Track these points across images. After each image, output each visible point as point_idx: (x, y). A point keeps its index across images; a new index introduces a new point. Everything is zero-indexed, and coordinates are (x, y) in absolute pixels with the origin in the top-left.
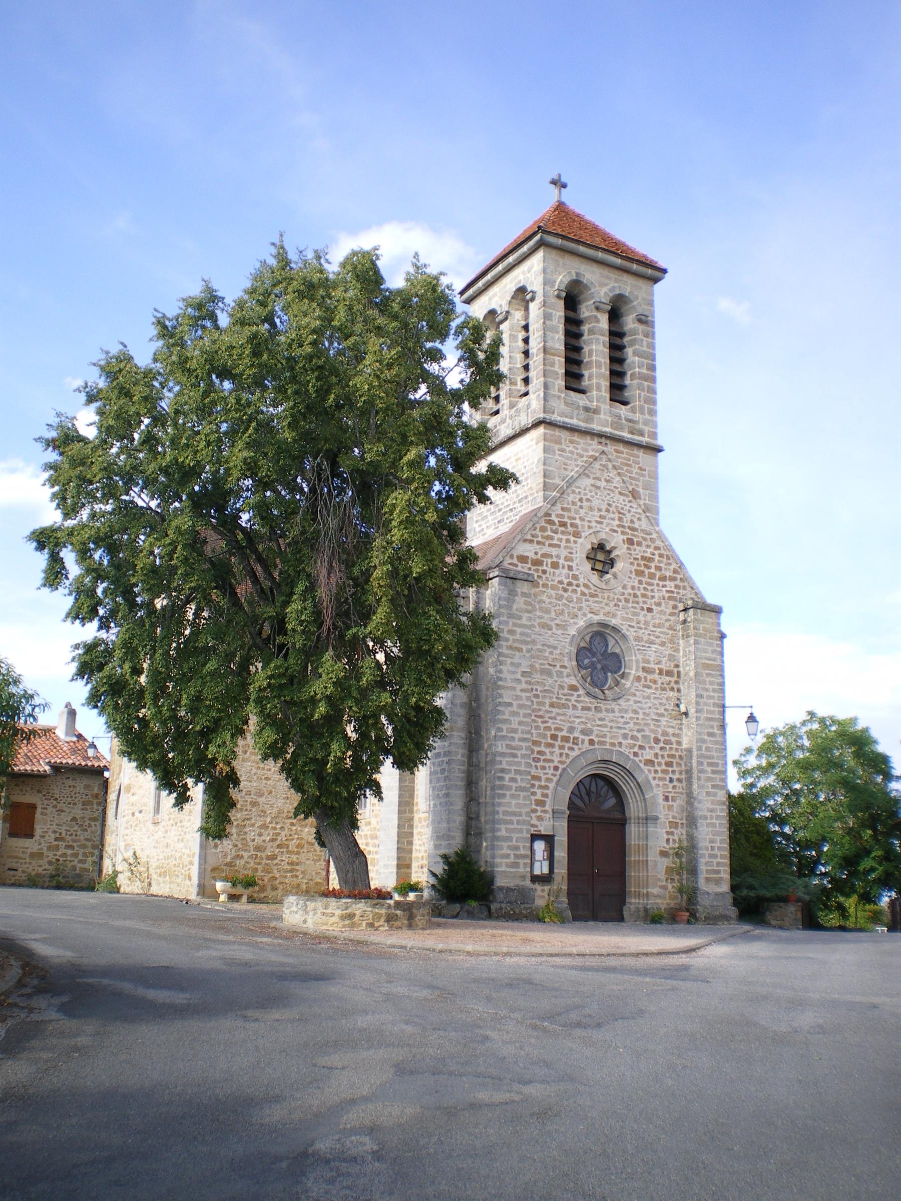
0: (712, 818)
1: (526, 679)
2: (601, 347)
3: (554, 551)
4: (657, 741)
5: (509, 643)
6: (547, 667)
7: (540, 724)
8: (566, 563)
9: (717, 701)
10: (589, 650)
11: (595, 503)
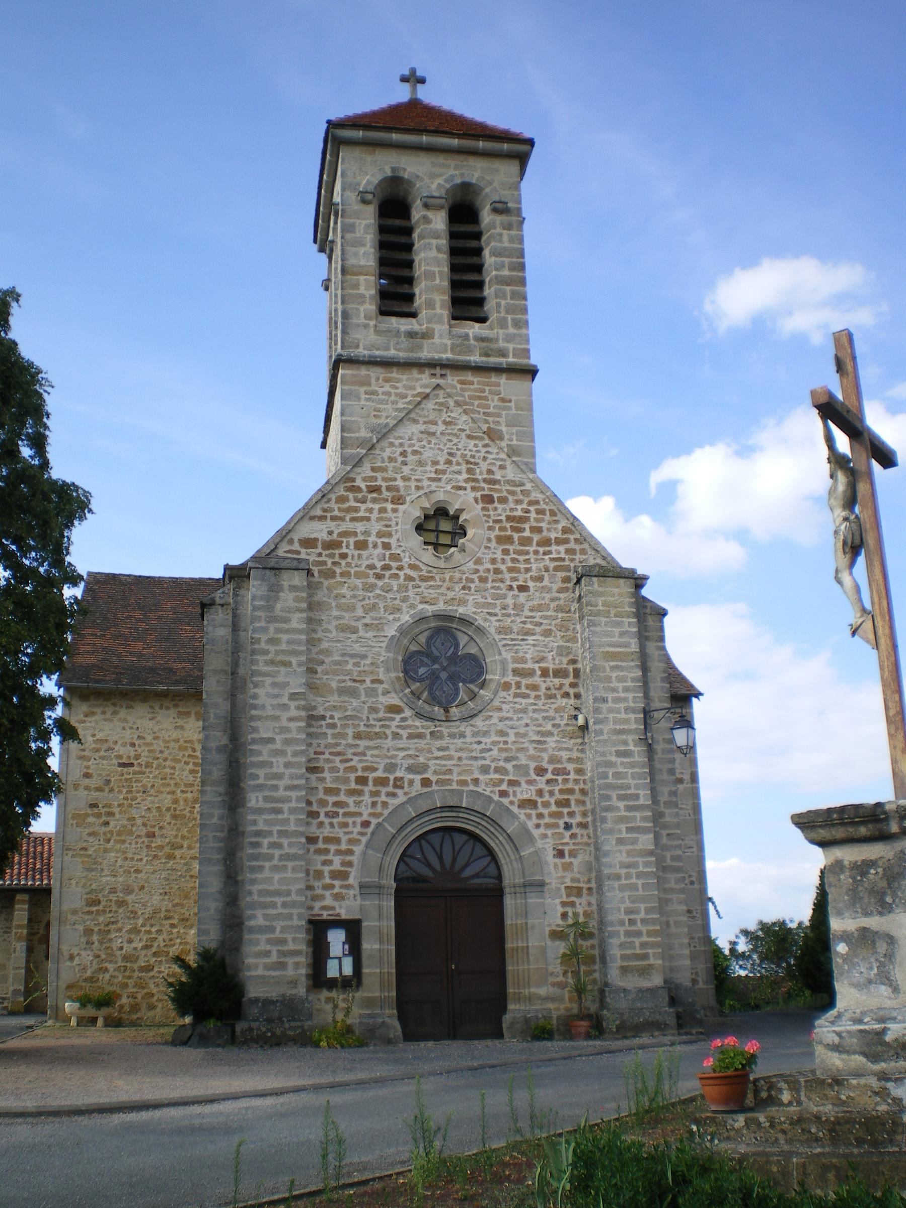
0: (628, 876)
1: (297, 703)
2: (434, 253)
3: (360, 527)
4: (541, 771)
5: (271, 656)
6: (350, 684)
7: (338, 764)
8: (379, 541)
9: (632, 705)
10: (428, 655)
11: (428, 454)
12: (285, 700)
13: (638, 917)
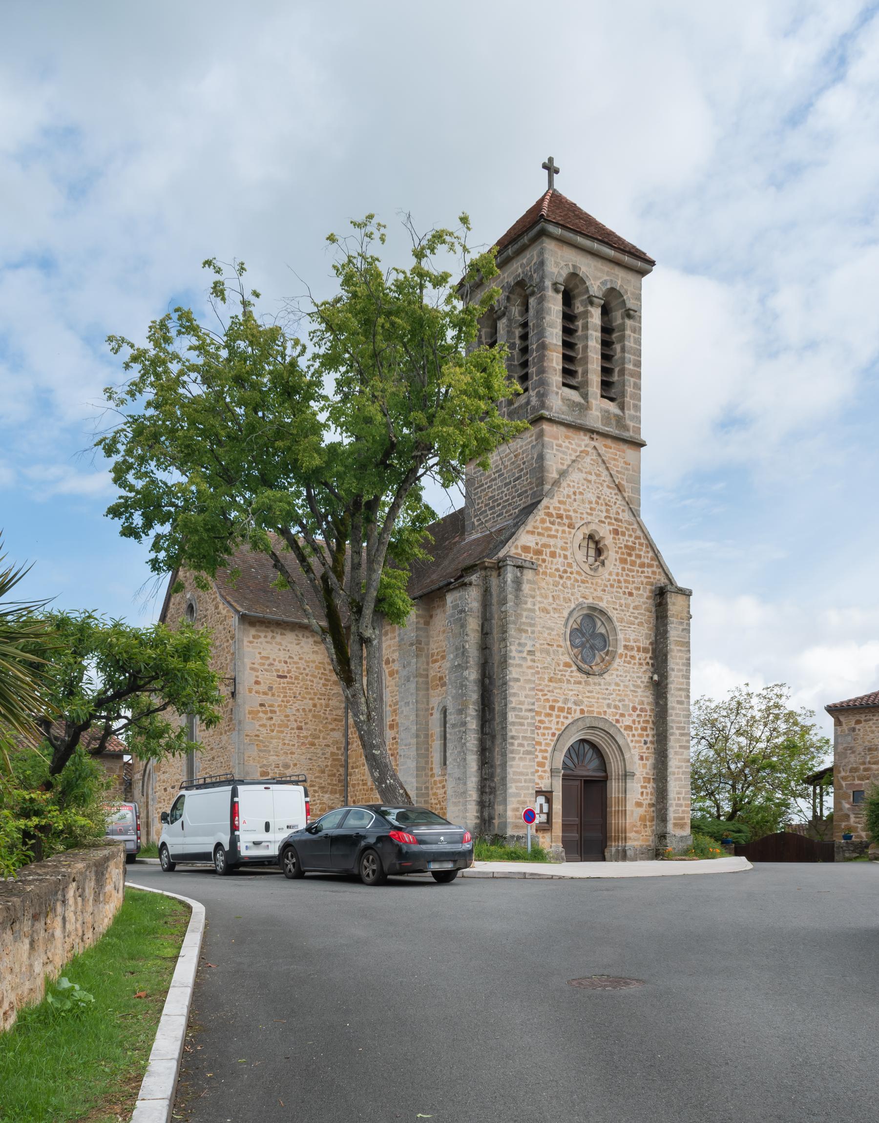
3: (552, 542)
6: (546, 646)
8: (562, 552)
12: (525, 655)
13: (681, 796)
